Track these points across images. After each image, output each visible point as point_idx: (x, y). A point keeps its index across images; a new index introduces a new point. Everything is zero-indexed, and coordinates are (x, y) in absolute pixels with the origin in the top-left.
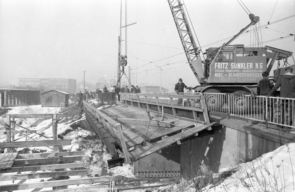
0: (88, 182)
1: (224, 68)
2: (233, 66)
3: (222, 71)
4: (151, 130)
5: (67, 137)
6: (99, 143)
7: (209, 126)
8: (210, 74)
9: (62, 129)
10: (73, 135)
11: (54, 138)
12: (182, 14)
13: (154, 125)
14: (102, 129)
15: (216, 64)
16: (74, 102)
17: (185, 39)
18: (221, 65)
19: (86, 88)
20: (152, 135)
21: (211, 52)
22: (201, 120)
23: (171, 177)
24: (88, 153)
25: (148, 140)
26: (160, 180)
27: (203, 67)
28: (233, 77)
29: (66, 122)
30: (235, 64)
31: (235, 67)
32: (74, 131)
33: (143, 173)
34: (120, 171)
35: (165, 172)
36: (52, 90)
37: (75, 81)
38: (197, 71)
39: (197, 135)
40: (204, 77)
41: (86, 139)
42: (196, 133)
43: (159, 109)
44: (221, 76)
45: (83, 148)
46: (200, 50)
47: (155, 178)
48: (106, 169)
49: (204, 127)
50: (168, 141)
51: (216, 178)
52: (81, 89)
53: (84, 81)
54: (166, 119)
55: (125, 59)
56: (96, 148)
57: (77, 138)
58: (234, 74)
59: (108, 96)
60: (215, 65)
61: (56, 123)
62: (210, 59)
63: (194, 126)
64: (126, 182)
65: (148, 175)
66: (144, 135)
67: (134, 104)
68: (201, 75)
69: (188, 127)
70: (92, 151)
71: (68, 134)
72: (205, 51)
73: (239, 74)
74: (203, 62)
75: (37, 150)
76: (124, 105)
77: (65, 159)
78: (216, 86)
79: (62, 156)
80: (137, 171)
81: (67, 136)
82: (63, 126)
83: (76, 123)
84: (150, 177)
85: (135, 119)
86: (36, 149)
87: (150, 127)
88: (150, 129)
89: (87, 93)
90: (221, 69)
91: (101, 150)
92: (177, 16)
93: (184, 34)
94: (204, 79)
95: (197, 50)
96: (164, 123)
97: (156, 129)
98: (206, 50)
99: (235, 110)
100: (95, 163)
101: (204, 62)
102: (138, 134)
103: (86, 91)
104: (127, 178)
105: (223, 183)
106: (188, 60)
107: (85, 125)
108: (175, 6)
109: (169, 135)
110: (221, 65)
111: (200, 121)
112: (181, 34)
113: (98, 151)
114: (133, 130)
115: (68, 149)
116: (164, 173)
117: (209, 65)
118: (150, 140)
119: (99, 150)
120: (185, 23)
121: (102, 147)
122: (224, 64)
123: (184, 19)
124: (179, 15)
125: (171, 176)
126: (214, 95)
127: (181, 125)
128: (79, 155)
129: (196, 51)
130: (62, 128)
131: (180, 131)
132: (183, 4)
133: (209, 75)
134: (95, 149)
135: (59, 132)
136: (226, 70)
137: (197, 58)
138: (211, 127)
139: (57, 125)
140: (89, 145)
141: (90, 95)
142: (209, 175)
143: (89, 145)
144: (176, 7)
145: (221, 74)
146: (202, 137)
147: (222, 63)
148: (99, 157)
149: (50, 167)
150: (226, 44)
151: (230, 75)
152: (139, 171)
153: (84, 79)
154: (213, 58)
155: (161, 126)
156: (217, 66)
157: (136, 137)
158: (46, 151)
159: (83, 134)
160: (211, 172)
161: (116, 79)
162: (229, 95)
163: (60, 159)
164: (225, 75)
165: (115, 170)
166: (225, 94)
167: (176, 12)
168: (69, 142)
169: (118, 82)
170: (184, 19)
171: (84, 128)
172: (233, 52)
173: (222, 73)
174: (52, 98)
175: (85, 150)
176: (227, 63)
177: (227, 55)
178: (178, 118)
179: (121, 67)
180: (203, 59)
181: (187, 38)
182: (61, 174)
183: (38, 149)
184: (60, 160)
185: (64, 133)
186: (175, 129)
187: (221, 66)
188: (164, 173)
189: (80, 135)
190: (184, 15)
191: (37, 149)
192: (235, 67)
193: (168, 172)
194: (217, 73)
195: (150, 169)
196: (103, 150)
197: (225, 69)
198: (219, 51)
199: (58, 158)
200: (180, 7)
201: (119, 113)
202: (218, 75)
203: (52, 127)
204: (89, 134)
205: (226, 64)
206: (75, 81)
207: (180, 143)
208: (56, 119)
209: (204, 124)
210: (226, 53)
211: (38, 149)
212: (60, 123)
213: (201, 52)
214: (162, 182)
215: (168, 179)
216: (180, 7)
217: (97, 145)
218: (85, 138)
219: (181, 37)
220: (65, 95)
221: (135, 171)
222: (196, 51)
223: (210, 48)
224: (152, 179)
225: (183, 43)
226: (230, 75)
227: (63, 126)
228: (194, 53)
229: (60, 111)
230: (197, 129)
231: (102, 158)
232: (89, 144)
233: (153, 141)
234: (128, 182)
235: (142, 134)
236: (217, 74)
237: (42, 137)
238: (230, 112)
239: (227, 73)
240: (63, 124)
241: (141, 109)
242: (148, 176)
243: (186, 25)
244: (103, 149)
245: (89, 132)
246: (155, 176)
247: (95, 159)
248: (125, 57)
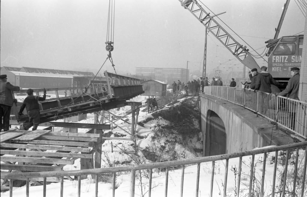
1: (283, 61)
2: (294, 59)
15: (273, 57)
30: (296, 57)
36: (150, 79)
44: (279, 70)
60: (273, 58)
71: (149, 122)
75: (118, 134)
81: (147, 124)
83: (157, 112)
86: (117, 133)
90: (279, 63)
100: (168, 152)
103: (179, 81)
122: (283, 57)
134: (168, 138)
136: (285, 64)
145: (279, 68)
147: (280, 57)
148: (171, 147)
153: (205, 65)
156: (275, 59)
158: (125, 136)
161: (202, 71)
164: (285, 69)
172: (295, 43)
173: (280, 68)
176: (286, 55)
182: (58, 148)
183: (119, 134)
191: (118, 133)
197: (284, 63)
202: (276, 69)
205: (286, 57)
206: (187, 71)
211: (119, 134)
220: (161, 85)
223: (270, 40)
226: (279, 69)
231: (174, 148)
236: (275, 69)
237: (126, 123)
245: (169, 121)
247: (167, 148)
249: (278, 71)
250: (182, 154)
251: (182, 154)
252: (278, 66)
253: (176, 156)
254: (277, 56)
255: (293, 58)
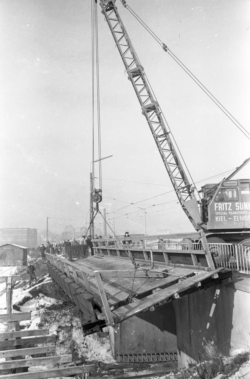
0: (55, 375)
1: (226, 210)
2: (238, 206)
3: (225, 213)
4: (138, 282)
5: (25, 307)
6: (66, 315)
7: (215, 273)
8: (209, 217)
9: (19, 296)
10: (32, 306)
11: (8, 309)
12: (169, 143)
13: (140, 276)
14: (73, 285)
15: (216, 204)
16: (34, 259)
17: (174, 174)
18: (222, 206)
19: (50, 240)
20: (140, 289)
21: (208, 190)
22: (202, 266)
23: (165, 361)
24: (53, 330)
25: (135, 295)
26: (150, 366)
27: (199, 208)
28: (240, 221)
29: (24, 287)
31: (241, 207)
32: (33, 299)
33: (127, 355)
34: (95, 354)
35: (157, 354)
37: (35, 230)
38: (191, 214)
39: (200, 285)
40: (202, 222)
41: (50, 310)
42: (199, 282)
43: (145, 256)
44: (223, 220)
45: (46, 323)
46: (194, 187)
47: (143, 363)
48: (76, 351)
49: (208, 275)
50: (161, 296)
51: (228, 365)
52: (43, 241)
53: (47, 230)
54: (155, 268)
55: (99, 194)
56: (62, 322)
57: (38, 309)
58: (240, 216)
59: (79, 250)
60: (215, 205)
61: (11, 288)
62: (208, 199)
63: (194, 274)
64: (104, 370)
65: (134, 360)
66: (128, 289)
67: (111, 253)
68: (198, 219)
69: (188, 276)
70: (58, 326)
71: (26, 303)
72: (200, 189)
73: (247, 216)
74: (198, 202)
76: (98, 255)
77: (24, 341)
78: (218, 233)
79: (19, 337)
80: (118, 353)
81: (25, 306)
82: (21, 293)
83: (36, 287)
84: (136, 361)
85: (115, 271)
87: (136, 279)
88: (136, 281)
89: (51, 246)
90: (222, 211)
91: (70, 325)
92: (162, 146)
93: (172, 168)
94: (202, 224)
95: (191, 188)
96: (155, 272)
97: (144, 282)
98: (202, 188)
99: (245, 264)
100: (62, 343)
101: (200, 202)
102: (120, 289)
103: (49, 244)
104: (106, 365)
105: (238, 372)
106: (180, 200)
107: (49, 290)
108: (159, 134)
109: (163, 287)
110: (222, 206)
111: (201, 267)
112: (169, 168)
113: (66, 326)
114: (114, 285)
115: (26, 325)
116: (156, 355)
117: (207, 206)
118: (137, 295)
119: (67, 324)
120: (173, 155)
121: (71, 320)
122: (226, 204)
123: (171, 150)
124: (165, 145)
125: (165, 360)
126: (216, 245)
127: (177, 274)
128: (41, 334)
129: (189, 189)
130: (19, 295)
131: (177, 281)
132: (170, 133)
133: (208, 218)
135: (15, 301)
136: (229, 212)
137: (191, 198)
138: (217, 274)
139: (12, 292)
140: (54, 317)
141: (55, 248)
142: (217, 359)
143: (54, 317)
144: (160, 135)
145: (223, 218)
146: (207, 288)
147: (223, 204)
148: (67, 335)
149: (4, 354)
150: (227, 179)
151: (235, 219)
152: (122, 354)
153: (47, 228)
154: (211, 197)
155: (151, 276)
156: (217, 207)
157: (118, 293)
159: (46, 302)
160: (220, 356)
162: (236, 246)
163: (17, 341)
164: (229, 219)
165: (89, 352)
166: (230, 244)
167: (160, 141)
168: (28, 316)
169: (90, 223)
170: (171, 150)
171: (46, 294)
172: (237, 189)
173: (224, 217)
174: (5, 255)
175: (48, 325)
177: (229, 192)
178: (172, 266)
179: (95, 204)
180: (198, 199)
181: (176, 173)
184: (17, 343)
185: (21, 303)
186: (169, 280)
187: (222, 207)
188: (156, 355)
189: (43, 304)
190: (171, 145)
192: (241, 207)
193: (161, 354)
194: (218, 217)
195: (136, 349)
196: (72, 325)
197: (228, 211)
198: (219, 187)
199: (14, 341)
200: (166, 135)
201: (93, 265)
203: (5, 294)
204: (54, 303)
206: (35, 230)
207: (179, 297)
208: (11, 283)
209: (208, 271)
210: (228, 190)
212: (17, 288)
213: (195, 190)
214: (154, 369)
215: (161, 365)
216: (166, 136)
217: (64, 318)
218: (49, 308)
219: (169, 172)
220: (22, 251)
221: (115, 353)
222: (189, 189)
223: (207, 184)
224: (138, 365)
225: (172, 179)
226: (223, 219)
227: (21, 293)
228: (187, 192)
229: (16, 272)
230: (199, 278)
231: (71, 336)
232: (54, 316)
233: (142, 296)
234: (107, 370)
235: (125, 288)
236: (218, 218)
238: (240, 267)
239: (232, 216)
240: (20, 289)
241: (121, 258)
242: (133, 361)
243: (174, 157)
244: (73, 324)
245: (54, 299)
246: (143, 361)
247: (61, 338)
248: (99, 191)
249: (223, 221)
250: (83, 343)
251: (83, 343)
252: (222, 216)
253: (75, 348)
254: (219, 203)
255: (237, 205)
